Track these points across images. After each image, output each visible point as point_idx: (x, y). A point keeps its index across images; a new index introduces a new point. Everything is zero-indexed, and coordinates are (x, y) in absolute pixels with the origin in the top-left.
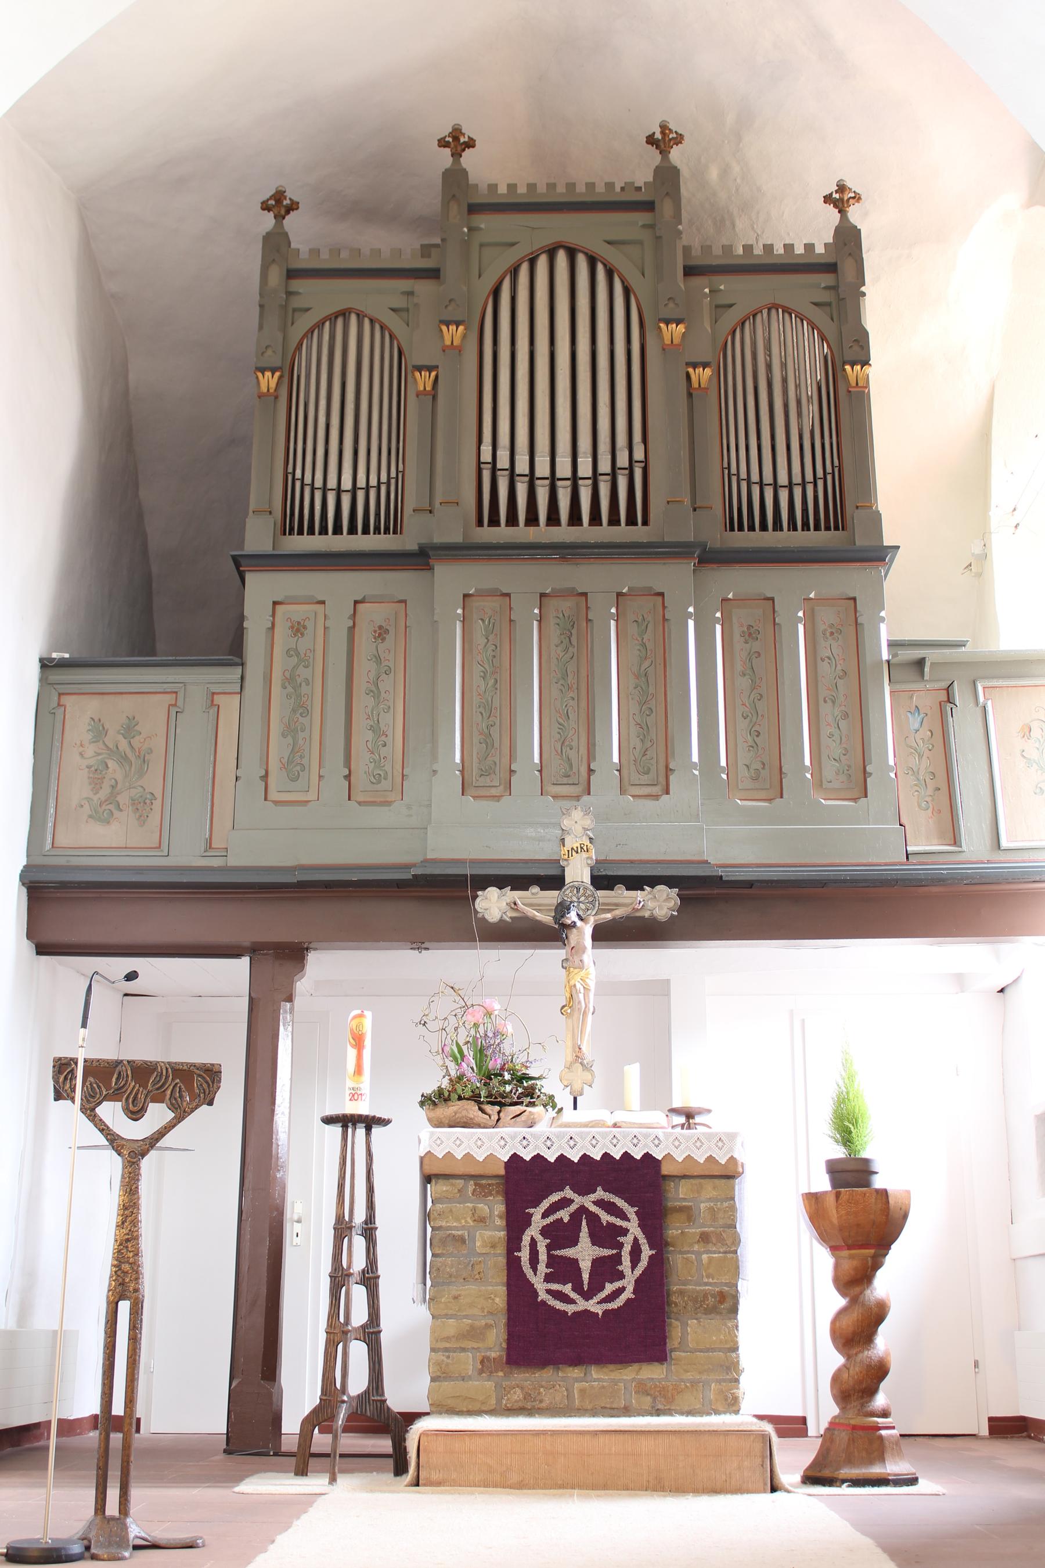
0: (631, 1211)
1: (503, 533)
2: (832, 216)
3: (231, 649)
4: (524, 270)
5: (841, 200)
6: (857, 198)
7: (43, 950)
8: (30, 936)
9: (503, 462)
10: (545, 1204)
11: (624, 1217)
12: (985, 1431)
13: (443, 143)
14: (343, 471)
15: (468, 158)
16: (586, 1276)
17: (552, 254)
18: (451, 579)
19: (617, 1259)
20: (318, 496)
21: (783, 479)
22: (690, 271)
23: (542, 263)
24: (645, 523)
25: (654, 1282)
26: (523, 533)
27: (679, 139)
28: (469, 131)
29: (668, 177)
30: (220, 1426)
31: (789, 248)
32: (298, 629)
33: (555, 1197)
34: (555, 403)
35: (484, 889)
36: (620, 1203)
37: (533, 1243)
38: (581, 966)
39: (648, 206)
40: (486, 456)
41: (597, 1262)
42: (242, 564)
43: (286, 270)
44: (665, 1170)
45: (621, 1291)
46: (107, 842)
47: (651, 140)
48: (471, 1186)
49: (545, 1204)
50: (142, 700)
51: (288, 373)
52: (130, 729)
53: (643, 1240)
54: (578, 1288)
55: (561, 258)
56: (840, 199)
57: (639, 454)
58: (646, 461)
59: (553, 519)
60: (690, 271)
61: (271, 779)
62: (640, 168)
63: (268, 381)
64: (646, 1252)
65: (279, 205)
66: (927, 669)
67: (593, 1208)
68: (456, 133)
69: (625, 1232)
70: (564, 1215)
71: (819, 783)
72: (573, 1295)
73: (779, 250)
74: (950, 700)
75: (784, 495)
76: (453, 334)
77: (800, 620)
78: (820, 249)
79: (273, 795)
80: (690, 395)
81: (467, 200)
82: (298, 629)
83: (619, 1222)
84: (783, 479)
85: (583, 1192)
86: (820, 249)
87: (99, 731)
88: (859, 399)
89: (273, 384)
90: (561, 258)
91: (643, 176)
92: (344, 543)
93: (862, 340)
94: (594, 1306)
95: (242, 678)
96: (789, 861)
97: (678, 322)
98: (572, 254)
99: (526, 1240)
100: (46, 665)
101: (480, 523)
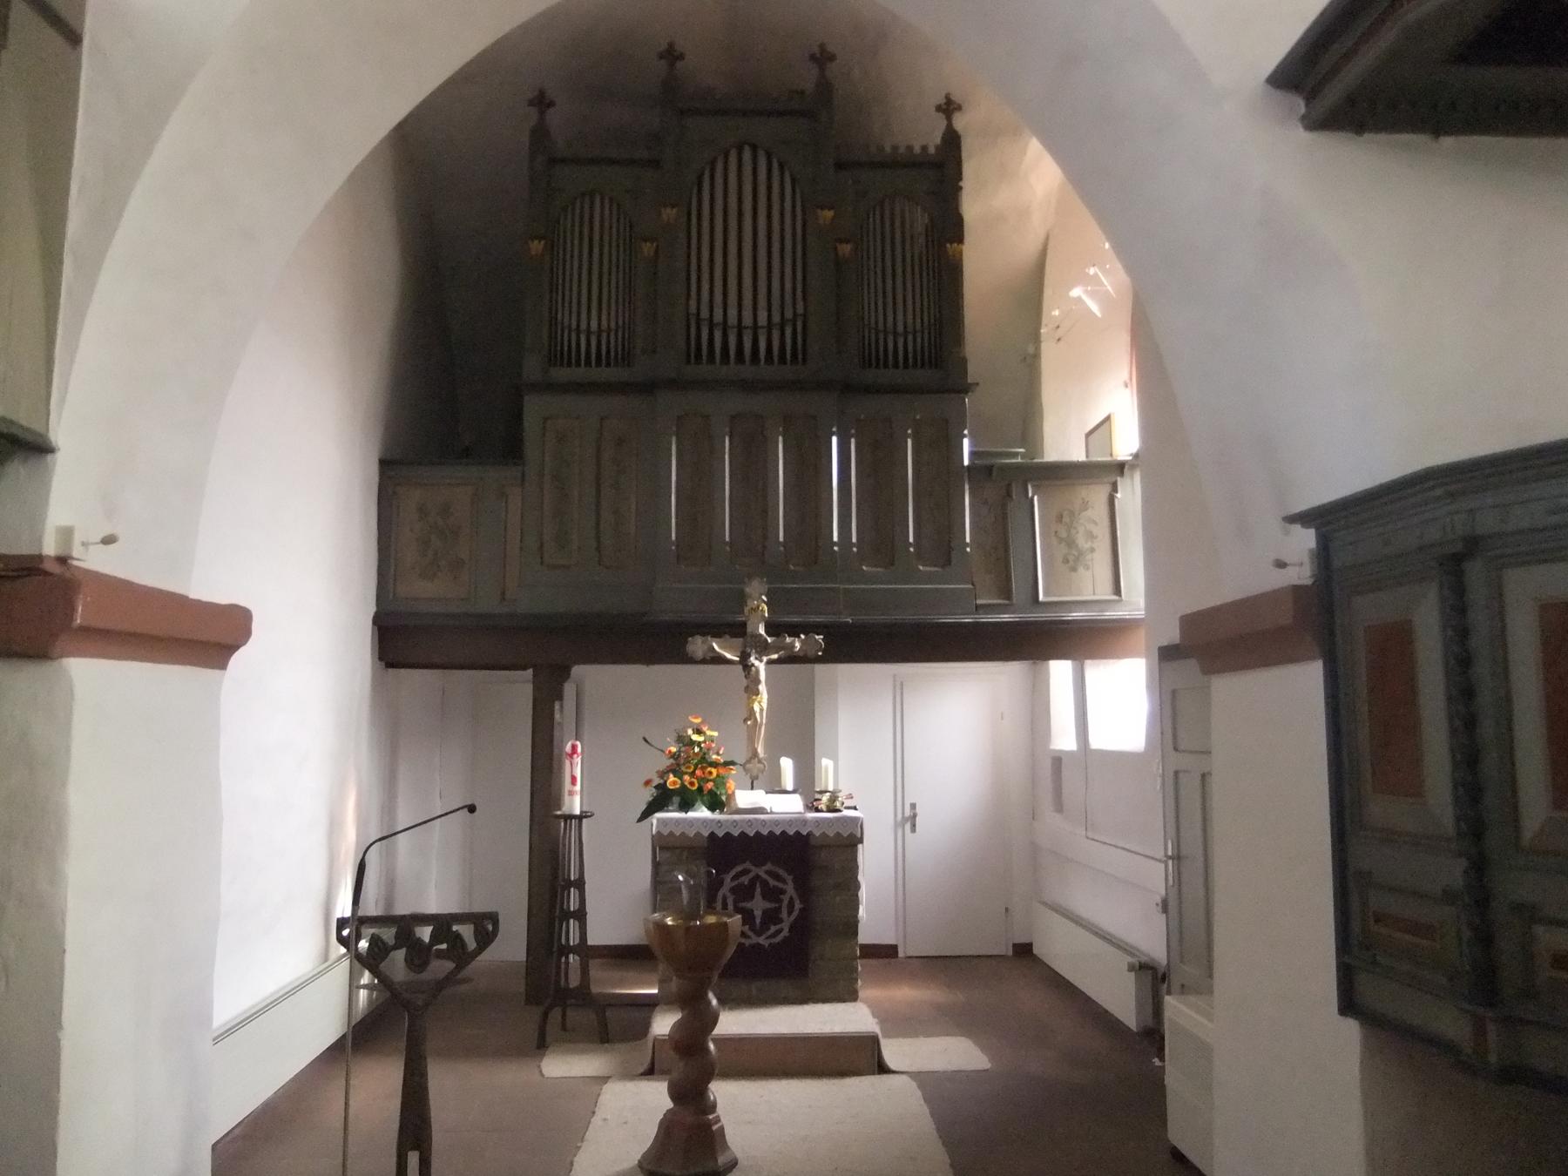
1: (704, 370)
3: (511, 450)
8: (380, 659)
9: (705, 314)
10: (733, 873)
11: (784, 882)
12: (1010, 953)
16: (758, 921)
19: (778, 910)
22: (840, 166)
24: (804, 360)
25: (803, 928)
27: (832, 58)
29: (825, 88)
30: (522, 989)
33: (739, 868)
36: (781, 872)
38: (757, 693)
40: (693, 309)
41: (765, 912)
43: (545, 153)
44: (812, 842)
45: (780, 931)
46: (429, 592)
49: (733, 873)
53: (795, 896)
54: (765, 884)
55: (747, 154)
56: (949, 108)
57: (800, 310)
58: (804, 315)
60: (840, 166)
62: (807, 79)
63: (537, 246)
64: (798, 905)
65: (542, 102)
69: (783, 892)
70: (745, 880)
71: (919, 556)
72: (750, 933)
74: (1009, 495)
76: (669, 214)
78: (932, 150)
83: (780, 885)
85: (758, 864)
86: (932, 150)
87: (422, 511)
90: (747, 154)
91: (809, 85)
93: (958, 223)
94: (762, 940)
96: (891, 735)
97: (830, 209)
98: (754, 148)
99: (720, 894)
100: (385, 464)
101: (688, 362)
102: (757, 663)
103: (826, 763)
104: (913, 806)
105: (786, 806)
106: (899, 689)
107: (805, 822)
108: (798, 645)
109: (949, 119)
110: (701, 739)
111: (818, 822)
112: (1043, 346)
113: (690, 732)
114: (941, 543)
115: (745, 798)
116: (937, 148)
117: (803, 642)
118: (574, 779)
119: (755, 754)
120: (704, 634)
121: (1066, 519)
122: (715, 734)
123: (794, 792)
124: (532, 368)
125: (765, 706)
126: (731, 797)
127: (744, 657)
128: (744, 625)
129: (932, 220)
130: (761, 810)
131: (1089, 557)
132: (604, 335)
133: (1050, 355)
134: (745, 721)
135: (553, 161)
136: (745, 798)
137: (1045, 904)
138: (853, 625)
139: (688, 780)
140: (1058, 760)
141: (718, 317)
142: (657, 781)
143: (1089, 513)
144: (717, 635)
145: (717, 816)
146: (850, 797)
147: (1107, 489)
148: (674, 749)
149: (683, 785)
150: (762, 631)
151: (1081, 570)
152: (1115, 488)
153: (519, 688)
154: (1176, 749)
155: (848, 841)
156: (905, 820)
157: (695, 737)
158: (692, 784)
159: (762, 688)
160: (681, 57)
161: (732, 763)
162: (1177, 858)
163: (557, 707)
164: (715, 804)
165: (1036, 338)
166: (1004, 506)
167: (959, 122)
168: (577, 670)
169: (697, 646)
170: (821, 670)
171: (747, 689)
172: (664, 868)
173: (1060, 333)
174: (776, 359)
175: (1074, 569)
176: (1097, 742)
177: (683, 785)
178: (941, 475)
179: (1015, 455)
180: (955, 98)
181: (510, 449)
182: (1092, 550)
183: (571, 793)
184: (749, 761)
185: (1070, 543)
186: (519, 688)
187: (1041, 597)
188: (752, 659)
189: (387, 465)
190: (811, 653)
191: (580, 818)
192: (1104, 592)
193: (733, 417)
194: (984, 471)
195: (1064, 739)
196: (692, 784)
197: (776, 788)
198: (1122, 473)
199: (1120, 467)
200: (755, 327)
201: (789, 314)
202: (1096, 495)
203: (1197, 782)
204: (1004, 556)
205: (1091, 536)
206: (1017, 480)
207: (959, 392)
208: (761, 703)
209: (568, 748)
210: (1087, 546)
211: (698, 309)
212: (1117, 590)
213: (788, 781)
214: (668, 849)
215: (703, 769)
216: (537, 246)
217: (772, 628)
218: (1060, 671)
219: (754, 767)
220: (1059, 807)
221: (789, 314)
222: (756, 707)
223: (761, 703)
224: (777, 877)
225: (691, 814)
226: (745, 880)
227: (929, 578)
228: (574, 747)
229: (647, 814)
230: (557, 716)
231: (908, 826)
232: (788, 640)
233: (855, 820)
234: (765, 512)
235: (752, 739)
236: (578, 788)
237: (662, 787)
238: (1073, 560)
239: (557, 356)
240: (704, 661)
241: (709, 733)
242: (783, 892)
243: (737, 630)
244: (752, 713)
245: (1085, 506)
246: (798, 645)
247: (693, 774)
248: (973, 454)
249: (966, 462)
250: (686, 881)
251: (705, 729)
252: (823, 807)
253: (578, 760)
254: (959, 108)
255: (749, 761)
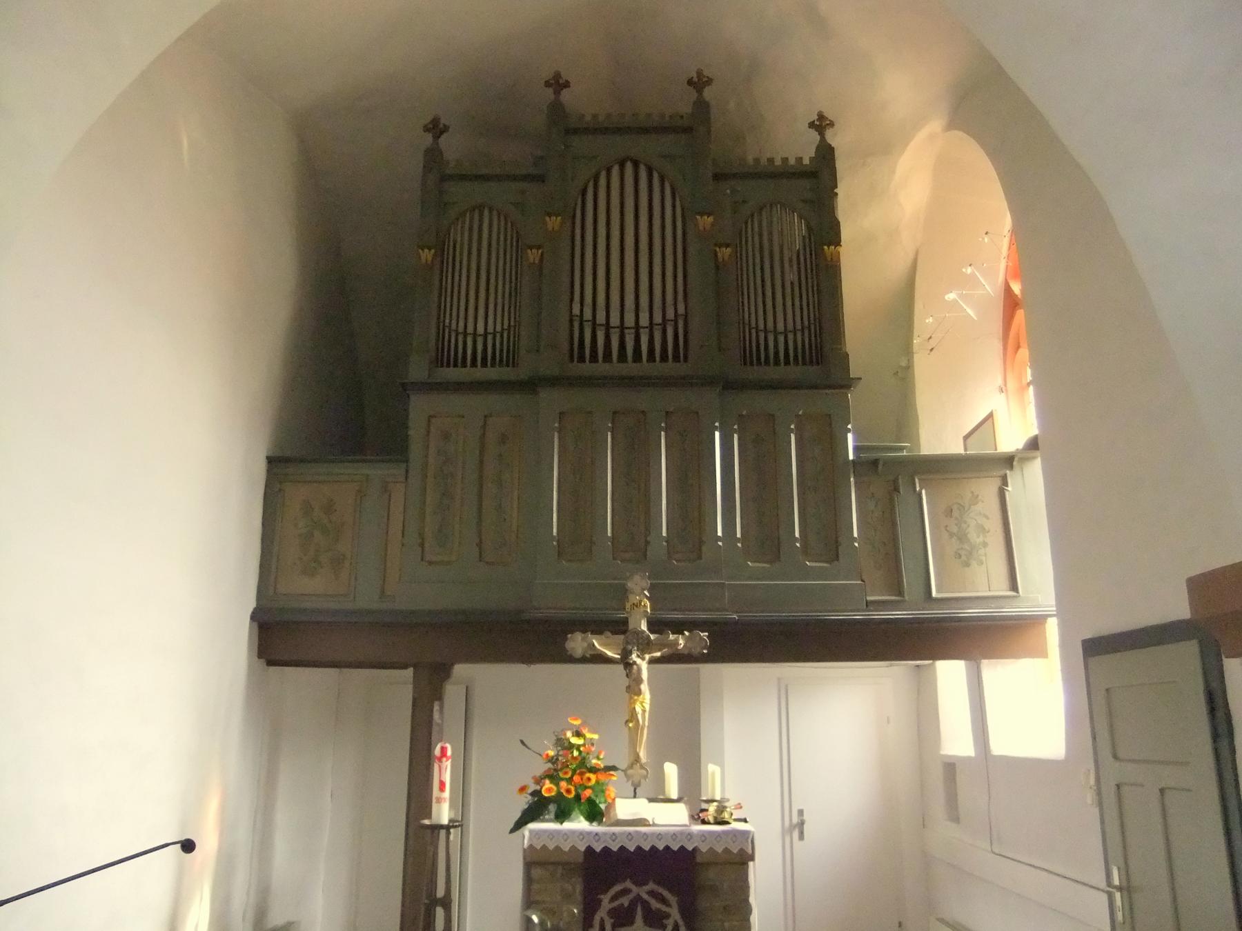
0: (672, 899)
1: (587, 368)
2: (814, 136)
4: (603, 174)
5: (820, 126)
6: (832, 124)
7: (270, 663)
9: (588, 314)
11: (669, 905)
13: (547, 84)
14: (478, 319)
15: (565, 95)
17: (622, 166)
18: (550, 399)
20: (461, 338)
21: (781, 327)
22: (717, 177)
23: (615, 171)
26: (601, 368)
27: (709, 81)
28: (565, 76)
29: (702, 107)
31: (785, 160)
32: (446, 436)
34: (627, 269)
35: (572, 632)
36: (666, 893)
37: (602, 920)
38: (639, 693)
39: (688, 130)
40: (576, 311)
42: (406, 389)
44: (699, 859)
46: (311, 589)
47: (690, 82)
48: (560, 870)
50: (340, 485)
51: (441, 247)
52: (329, 508)
53: (681, 923)
54: (645, 905)
55: (629, 167)
56: (821, 124)
57: (681, 310)
59: (622, 357)
61: (427, 545)
62: (684, 105)
63: (427, 255)
65: (436, 128)
66: (880, 467)
67: (645, 897)
68: (557, 76)
69: (668, 916)
70: (625, 901)
71: (805, 549)
73: (778, 162)
74: (896, 490)
75: (781, 339)
76: (553, 223)
77: (792, 431)
78: (806, 161)
79: (428, 557)
80: (717, 268)
81: (564, 125)
82: (446, 436)
84: (781, 327)
86: (806, 161)
87: (307, 509)
88: (833, 270)
89: (430, 259)
90: (629, 167)
91: (685, 108)
92: (480, 373)
93: (835, 227)
95: (407, 471)
96: (777, 734)
97: (709, 215)
98: (636, 164)
99: (597, 918)
100: (271, 461)
102: (639, 661)
103: (712, 770)
104: (801, 812)
105: (668, 818)
106: (784, 692)
107: (690, 836)
108: (681, 642)
109: (822, 134)
110: (580, 741)
111: (703, 835)
112: (916, 358)
113: (569, 734)
114: (829, 541)
115: (626, 808)
116: (811, 159)
117: (687, 640)
118: (442, 786)
119: (637, 759)
120: (584, 632)
121: (956, 513)
122: (596, 737)
123: (678, 800)
124: (418, 370)
125: (647, 707)
126: (611, 806)
127: (626, 654)
128: (625, 622)
129: (809, 229)
130: (642, 822)
131: (982, 551)
132: (490, 337)
133: (923, 365)
134: (627, 722)
135: (444, 178)
136: (626, 808)
137: (941, 920)
138: (736, 623)
139: (566, 788)
140: (951, 767)
141: (601, 318)
142: (533, 787)
143: (979, 507)
144: (598, 632)
145: (595, 827)
146: (739, 807)
147: (994, 484)
148: (551, 753)
149: (559, 794)
150: (644, 627)
151: (974, 564)
152: (1005, 483)
153: (399, 686)
154: (1115, 757)
155: (738, 859)
156: (792, 827)
157: (574, 740)
158: (568, 791)
159: (644, 687)
160: (567, 85)
161: (614, 768)
162: (1127, 889)
163: (436, 708)
164: (594, 814)
165: (908, 351)
166: (891, 500)
167: (832, 138)
168: (460, 670)
169: (577, 643)
170: (707, 670)
171: (628, 687)
172: (535, 886)
173: (932, 343)
174: (658, 359)
175: (967, 565)
176: (1000, 746)
177: (559, 794)
178: (826, 475)
179: (901, 449)
180: (829, 114)
181: (393, 446)
182: (985, 545)
183: (439, 800)
184: (631, 766)
185: (962, 537)
186: (399, 686)
187: (934, 594)
188: (634, 657)
189: (281, 468)
190: (696, 651)
191: (447, 828)
192: (1000, 587)
193: (615, 413)
194: (869, 465)
195: (957, 741)
196: (568, 791)
197: (658, 797)
198: (1011, 467)
199: (1009, 461)
200: (637, 327)
201: (670, 314)
202: (986, 489)
203: (1114, 789)
204: (893, 554)
205: (982, 530)
206: (898, 475)
207: (842, 387)
208: (644, 703)
209: (437, 751)
210: (981, 539)
211: (582, 311)
212: (1014, 587)
213: (673, 790)
214: (540, 866)
215: (582, 774)
216: (427, 255)
217: (655, 626)
218: (950, 674)
219: (637, 772)
220: (955, 817)
221: (670, 314)
222: (638, 709)
223: (644, 703)
224: (664, 901)
225: (567, 825)
226: (625, 901)
227: (821, 574)
228: (443, 750)
229: (520, 824)
230: (436, 716)
231: (796, 834)
232: (672, 637)
233: (745, 834)
234: (647, 512)
235: (633, 744)
236: (447, 794)
237: (537, 793)
238: (966, 556)
239: (442, 358)
240: (583, 660)
241: (589, 735)
242: (668, 916)
243: (619, 627)
244: (633, 716)
245: (975, 499)
246: (681, 642)
247: (570, 780)
248: (856, 449)
249: (851, 457)
250: (542, 923)
251: (585, 731)
252: (711, 819)
253: (447, 764)
254: (832, 124)
255: (631, 766)
